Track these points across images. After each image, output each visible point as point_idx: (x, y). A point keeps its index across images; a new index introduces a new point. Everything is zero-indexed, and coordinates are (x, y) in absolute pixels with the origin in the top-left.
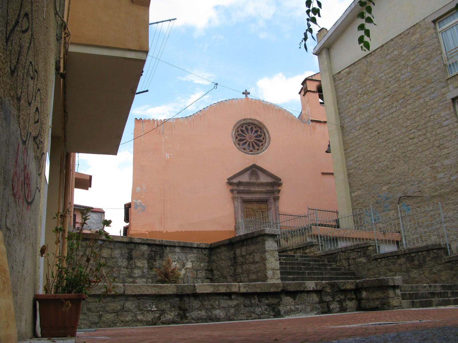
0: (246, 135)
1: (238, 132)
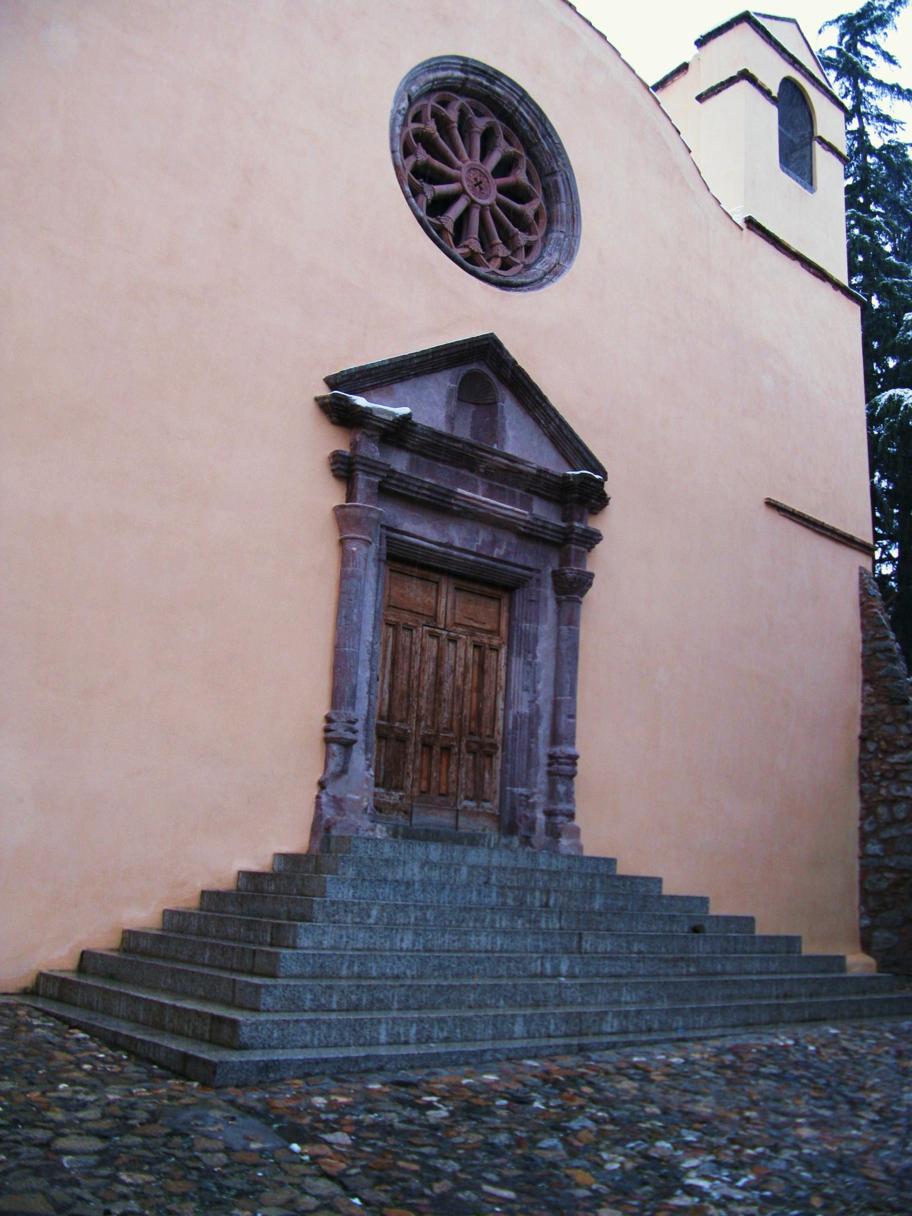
0: (459, 157)
1: (417, 118)
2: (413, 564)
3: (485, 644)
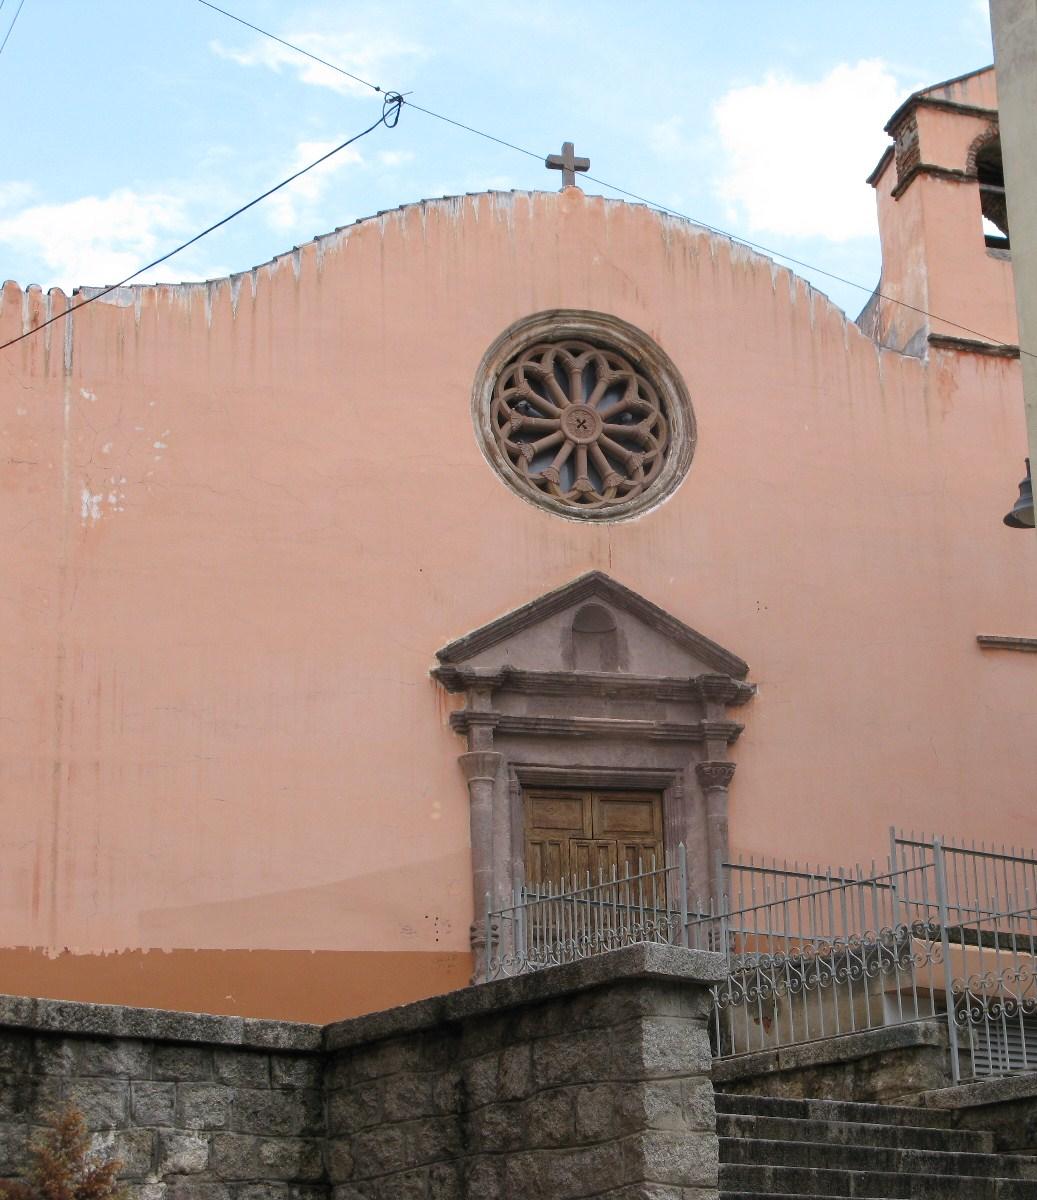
1: (510, 384)
2: (552, 788)
3: (637, 845)
